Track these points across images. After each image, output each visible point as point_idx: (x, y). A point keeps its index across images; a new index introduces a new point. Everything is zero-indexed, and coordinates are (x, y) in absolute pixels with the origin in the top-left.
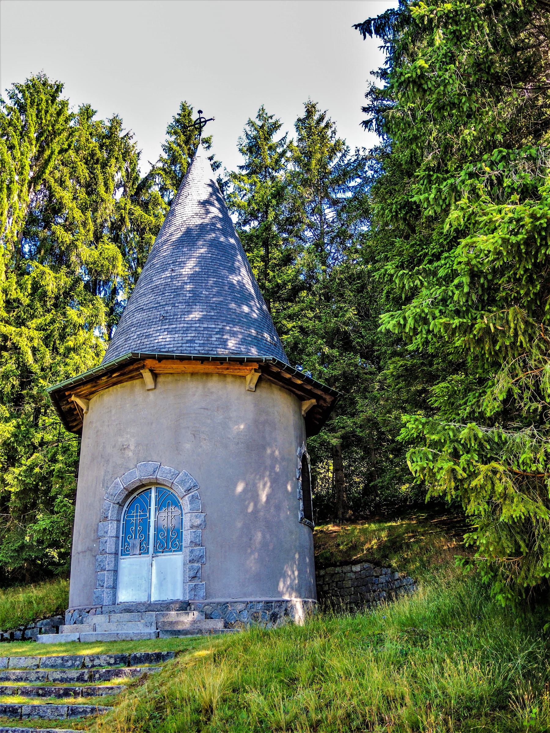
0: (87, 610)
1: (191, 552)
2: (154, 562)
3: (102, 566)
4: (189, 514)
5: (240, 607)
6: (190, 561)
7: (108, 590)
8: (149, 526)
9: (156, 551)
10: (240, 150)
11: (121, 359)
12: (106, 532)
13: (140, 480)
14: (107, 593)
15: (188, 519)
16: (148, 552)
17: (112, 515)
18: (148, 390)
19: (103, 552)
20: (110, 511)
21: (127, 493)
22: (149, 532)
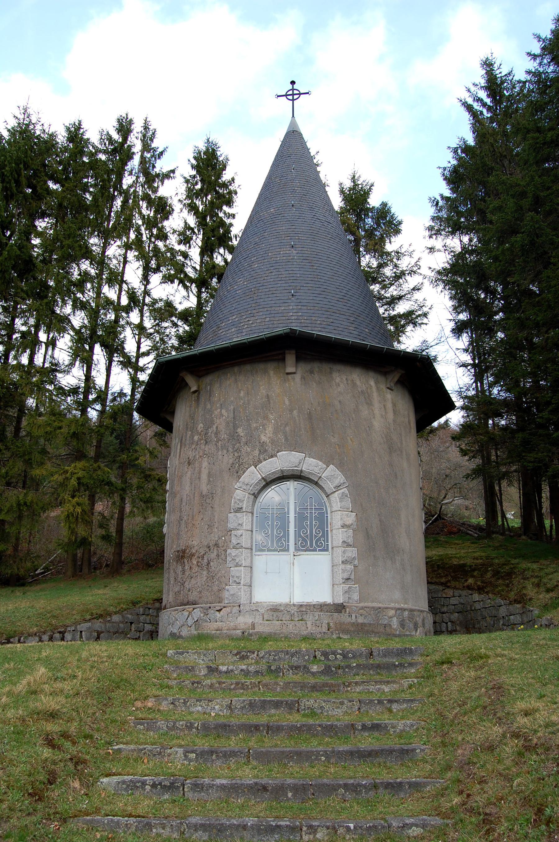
0: (218, 608)
1: (344, 552)
2: (295, 561)
3: (237, 561)
4: (339, 512)
5: (391, 613)
6: (343, 562)
7: (246, 587)
8: (289, 522)
9: (297, 549)
10: (118, 119)
11: (277, 333)
12: (241, 525)
13: (282, 471)
14: (245, 591)
15: (339, 517)
16: (288, 550)
17: (247, 506)
18: (288, 374)
19: (238, 546)
20: (245, 502)
21: (264, 483)
22: (288, 528)
